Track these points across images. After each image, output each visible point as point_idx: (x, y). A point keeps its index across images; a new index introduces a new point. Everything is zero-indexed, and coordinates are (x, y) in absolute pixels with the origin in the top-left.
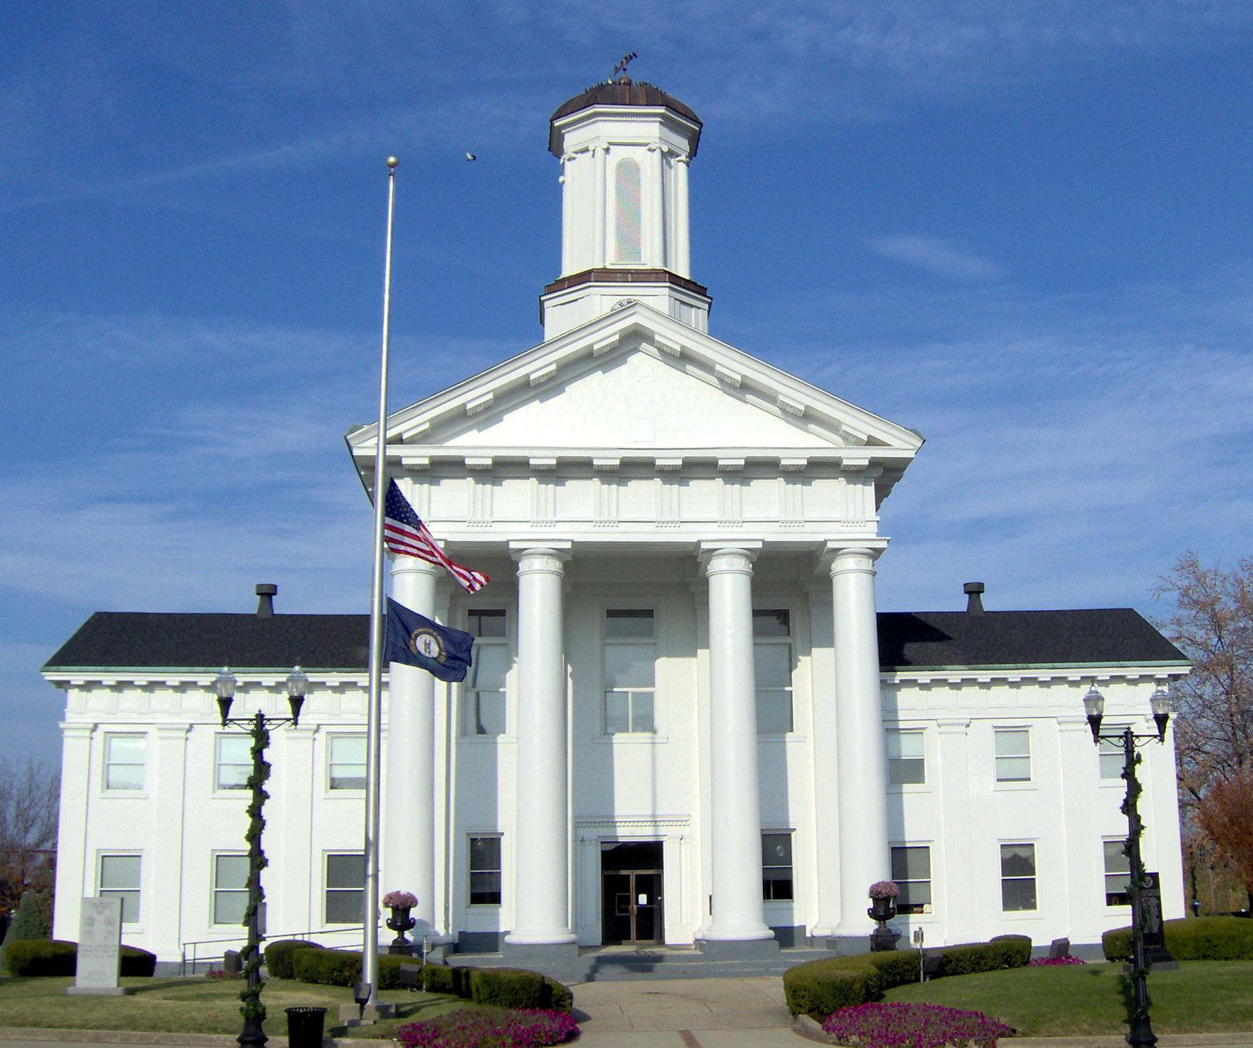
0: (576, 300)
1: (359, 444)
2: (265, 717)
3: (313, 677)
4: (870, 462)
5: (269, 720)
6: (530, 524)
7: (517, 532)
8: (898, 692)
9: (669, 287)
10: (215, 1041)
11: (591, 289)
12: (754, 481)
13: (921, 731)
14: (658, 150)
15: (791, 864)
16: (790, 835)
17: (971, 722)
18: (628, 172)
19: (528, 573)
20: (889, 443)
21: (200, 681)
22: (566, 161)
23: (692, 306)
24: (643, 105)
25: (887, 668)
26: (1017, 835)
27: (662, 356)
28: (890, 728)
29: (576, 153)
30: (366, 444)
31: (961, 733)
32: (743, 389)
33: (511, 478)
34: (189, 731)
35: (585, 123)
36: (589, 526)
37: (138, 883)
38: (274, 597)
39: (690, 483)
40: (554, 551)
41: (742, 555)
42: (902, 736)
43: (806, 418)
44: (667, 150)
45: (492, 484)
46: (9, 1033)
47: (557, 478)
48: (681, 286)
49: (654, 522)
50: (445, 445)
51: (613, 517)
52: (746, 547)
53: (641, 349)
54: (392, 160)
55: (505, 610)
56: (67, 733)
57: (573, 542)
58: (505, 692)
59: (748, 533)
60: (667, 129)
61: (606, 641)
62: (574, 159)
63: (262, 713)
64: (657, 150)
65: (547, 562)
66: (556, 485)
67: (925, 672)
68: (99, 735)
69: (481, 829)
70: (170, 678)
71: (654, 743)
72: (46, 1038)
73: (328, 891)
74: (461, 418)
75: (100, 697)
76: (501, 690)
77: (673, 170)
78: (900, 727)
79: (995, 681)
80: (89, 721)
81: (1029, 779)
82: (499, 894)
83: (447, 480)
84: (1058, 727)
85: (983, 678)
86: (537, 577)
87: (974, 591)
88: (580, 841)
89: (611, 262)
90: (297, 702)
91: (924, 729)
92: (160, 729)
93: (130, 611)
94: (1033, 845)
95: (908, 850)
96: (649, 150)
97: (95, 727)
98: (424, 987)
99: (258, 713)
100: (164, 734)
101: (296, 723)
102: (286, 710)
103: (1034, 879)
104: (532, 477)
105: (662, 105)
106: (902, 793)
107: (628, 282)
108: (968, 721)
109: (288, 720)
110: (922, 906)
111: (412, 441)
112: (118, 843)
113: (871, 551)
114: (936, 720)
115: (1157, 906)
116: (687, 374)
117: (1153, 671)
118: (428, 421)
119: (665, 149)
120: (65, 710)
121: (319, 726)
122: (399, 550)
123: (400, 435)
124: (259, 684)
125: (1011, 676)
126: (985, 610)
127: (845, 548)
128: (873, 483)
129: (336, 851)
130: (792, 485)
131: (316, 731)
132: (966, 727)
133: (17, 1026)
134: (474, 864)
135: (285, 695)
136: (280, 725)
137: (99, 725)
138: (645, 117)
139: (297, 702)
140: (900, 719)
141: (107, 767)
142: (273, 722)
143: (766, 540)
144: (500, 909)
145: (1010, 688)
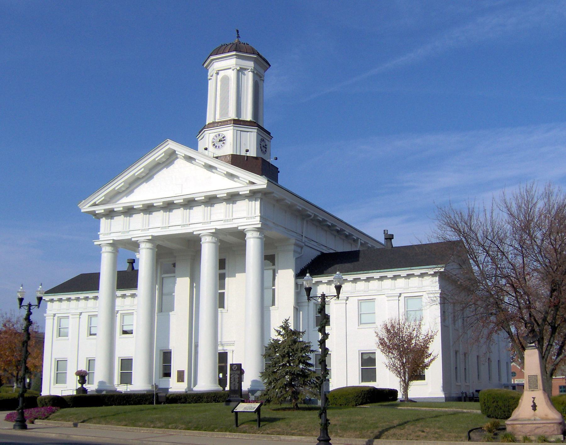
1: (83, 207)
2: (326, 295)
3: (345, 277)
5: (327, 296)
6: (160, 228)
7: (136, 234)
8: (318, 287)
12: (216, 205)
15: (171, 363)
23: (248, 132)
30: (85, 207)
33: (117, 216)
34: (347, 300)
35: (210, 65)
36: (159, 229)
37: (66, 370)
38: (392, 240)
40: (147, 240)
44: (239, 68)
47: (150, 212)
48: (241, 125)
50: (117, 203)
51: (167, 225)
52: (209, 232)
55: (225, 259)
56: (47, 318)
59: (213, 226)
60: (240, 60)
61: (163, 276)
62: (211, 79)
63: (324, 293)
64: (235, 69)
65: (212, 239)
68: (402, 298)
69: (165, 348)
71: (222, 313)
73: (362, 368)
74: (117, 194)
75: (56, 304)
76: (173, 294)
77: (246, 76)
80: (345, 296)
81: (375, 323)
82: (170, 373)
83: (135, 215)
86: (144, 250)
90: (338, 288)
92: (72, 315)
94: (375, 353)
97: (54, 315)
99: (322, 293)
100: (390, 298)
101: (338, 298)
102: (334, 292)
103: (132, 372)
104: (246, 199)
105: (234, 51)
109: (335, 296)
112: (60, 356)
115: (231, 383)
119: (238, 68)
120: (47, 310)
121: (400, 294)
123: (95, 202)
124: (413, 274)
125: (375, 276)
128: (259, 200)
129: (125, 357)
131: (400, 296)
133: (42, 420)
134: (220, 362)
135: (333, 285)
136: (332, 298)
137: (349, 297)
139: (338, 288)
141: (360, 315)
142: (328, 297)
144: (170, 379)
145: (327, 285)
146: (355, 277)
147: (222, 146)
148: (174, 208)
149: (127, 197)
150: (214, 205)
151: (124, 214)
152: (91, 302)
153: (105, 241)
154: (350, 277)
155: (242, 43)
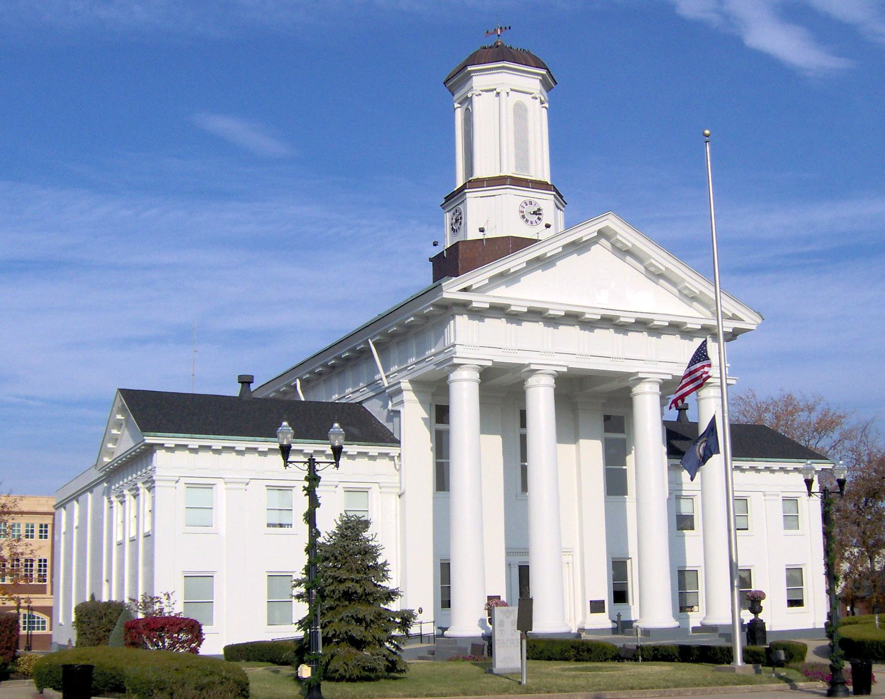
0: (494, 196)
4: (702, 327)
8: (682, 472)
9: (554, 195)
10: (738, 689)
11: (508, 189)
12: (663, 335)
13: (291, 489)
14: (539, 99)
16: (626, 562)
17: (179, 479)
18: (520, 111)
19: (535, 386)
20: (743, 319)
21: (261, 448)
22: (474, 95)
24: (533, 67)
25: (672, 456)
26: (794, 562)
27: (612, 248)
28: (675, 495)
29: (482, 91)
31: (172, 487)
32: (657, 275)
39: (523, 323)
41: (552, 375)
42: (681, 500)
43: (692, 298)
45: (516, 324)
46: (632, 694)
49: (610, 358)
50: (486, 294)
53: (599, 242)
54: (707, 132)
57: (673, 376)
58: (626, 469)
66: (479, 321)
67: (376, 447)
70: (239, 445)
72: (653, 696)
78: (683, 494)
79: (179, 447)
84: (225, 486)
85: (263, 448)
86: (713, 400)
87: (246, 381)
88: (509, 565)
89: (509, 171)
91: (294, 487)
93: (213, 394)
95: (686, 572)
96: (533, 98)
98: (640, 659)
104: (465, 314)
106: (684, 536)
107: (530, 188)
108: (248, 481)
110: (692, 607)
111: (477, 290)
113: (555, 372)
114: (379, 483)
116: (625, 262)
117: (785, 465)
118: (487, 278)
122: (692, 383)
126: (676, 420)
127: (646, 378)
130: (510, 324)
132: (176, 483)
138: (537, 76)
140: (684, 489)
143: (569, 366)
145: (369, 460)
146: (271, 447)
147: (536, 223)
148: (630, 329)
149: (507, 287)
150: (521, 323)
151: (508, 318)
152: (384, 464)
153: (540, 366)
154: (170, 441)
155: (506, 28)
